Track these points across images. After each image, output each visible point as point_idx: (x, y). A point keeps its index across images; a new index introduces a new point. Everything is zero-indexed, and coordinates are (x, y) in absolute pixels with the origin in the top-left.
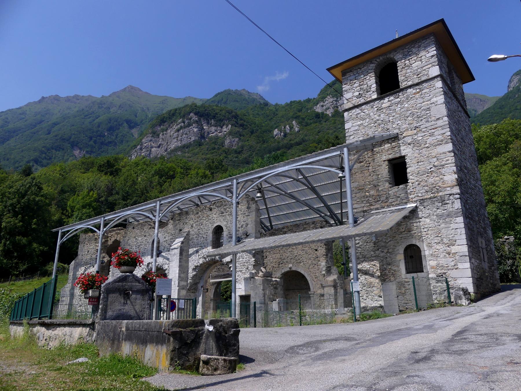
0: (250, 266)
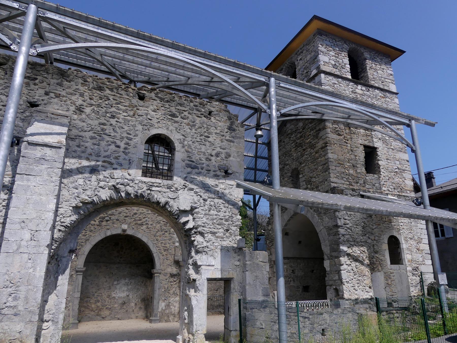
0: (234, 228)
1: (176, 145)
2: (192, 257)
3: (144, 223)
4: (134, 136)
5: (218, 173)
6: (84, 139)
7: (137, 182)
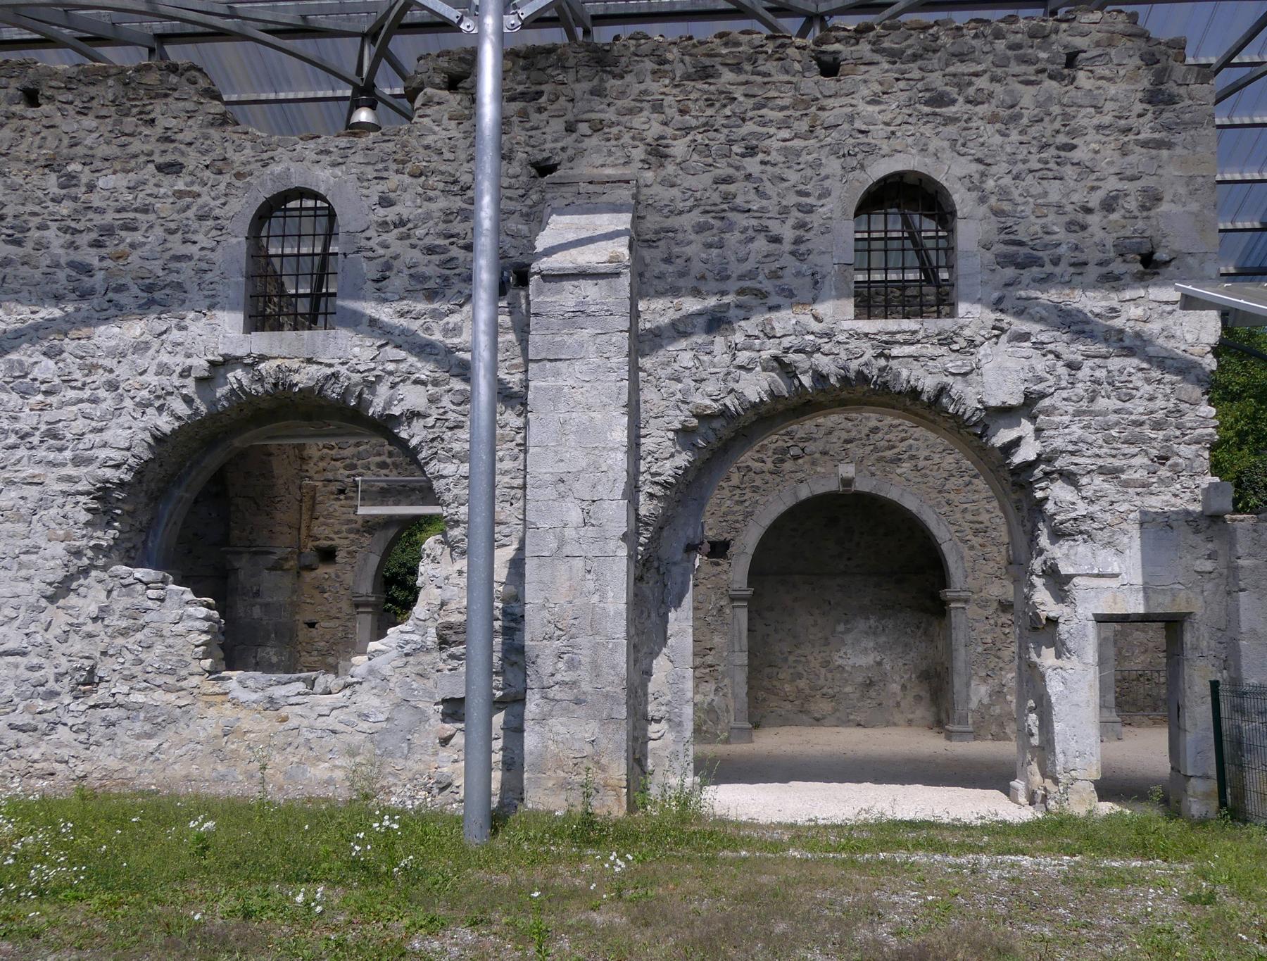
0: (1187, 451)
1: (956, 198)
2: (1041, 552)
3: (905, 456)
4: (820, 197)
5: (1118, 267)
6: (680, 236)
7: (841, 338)
